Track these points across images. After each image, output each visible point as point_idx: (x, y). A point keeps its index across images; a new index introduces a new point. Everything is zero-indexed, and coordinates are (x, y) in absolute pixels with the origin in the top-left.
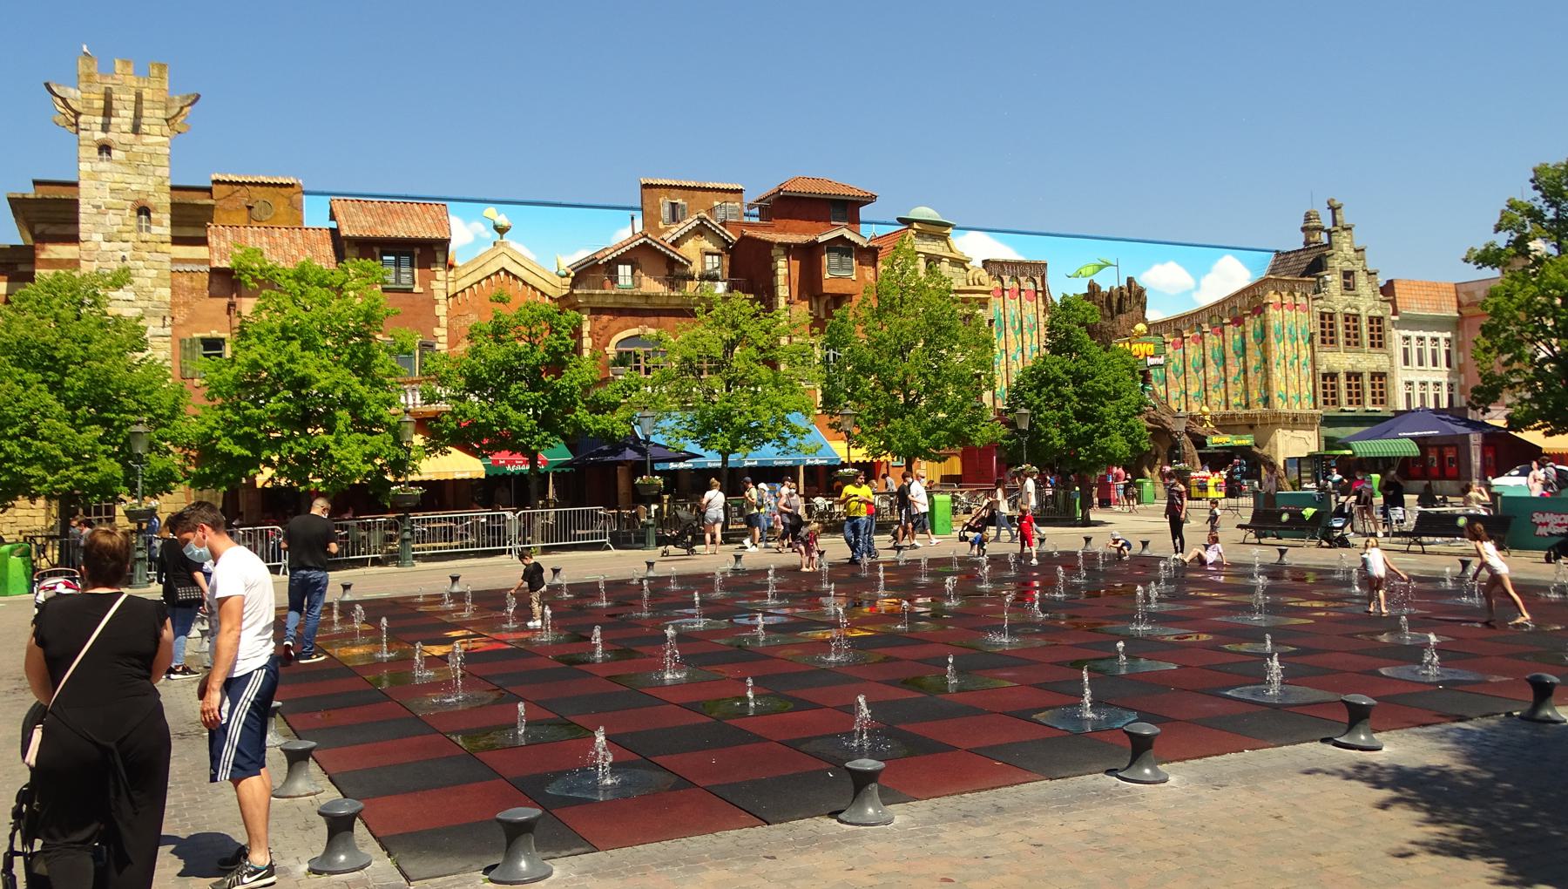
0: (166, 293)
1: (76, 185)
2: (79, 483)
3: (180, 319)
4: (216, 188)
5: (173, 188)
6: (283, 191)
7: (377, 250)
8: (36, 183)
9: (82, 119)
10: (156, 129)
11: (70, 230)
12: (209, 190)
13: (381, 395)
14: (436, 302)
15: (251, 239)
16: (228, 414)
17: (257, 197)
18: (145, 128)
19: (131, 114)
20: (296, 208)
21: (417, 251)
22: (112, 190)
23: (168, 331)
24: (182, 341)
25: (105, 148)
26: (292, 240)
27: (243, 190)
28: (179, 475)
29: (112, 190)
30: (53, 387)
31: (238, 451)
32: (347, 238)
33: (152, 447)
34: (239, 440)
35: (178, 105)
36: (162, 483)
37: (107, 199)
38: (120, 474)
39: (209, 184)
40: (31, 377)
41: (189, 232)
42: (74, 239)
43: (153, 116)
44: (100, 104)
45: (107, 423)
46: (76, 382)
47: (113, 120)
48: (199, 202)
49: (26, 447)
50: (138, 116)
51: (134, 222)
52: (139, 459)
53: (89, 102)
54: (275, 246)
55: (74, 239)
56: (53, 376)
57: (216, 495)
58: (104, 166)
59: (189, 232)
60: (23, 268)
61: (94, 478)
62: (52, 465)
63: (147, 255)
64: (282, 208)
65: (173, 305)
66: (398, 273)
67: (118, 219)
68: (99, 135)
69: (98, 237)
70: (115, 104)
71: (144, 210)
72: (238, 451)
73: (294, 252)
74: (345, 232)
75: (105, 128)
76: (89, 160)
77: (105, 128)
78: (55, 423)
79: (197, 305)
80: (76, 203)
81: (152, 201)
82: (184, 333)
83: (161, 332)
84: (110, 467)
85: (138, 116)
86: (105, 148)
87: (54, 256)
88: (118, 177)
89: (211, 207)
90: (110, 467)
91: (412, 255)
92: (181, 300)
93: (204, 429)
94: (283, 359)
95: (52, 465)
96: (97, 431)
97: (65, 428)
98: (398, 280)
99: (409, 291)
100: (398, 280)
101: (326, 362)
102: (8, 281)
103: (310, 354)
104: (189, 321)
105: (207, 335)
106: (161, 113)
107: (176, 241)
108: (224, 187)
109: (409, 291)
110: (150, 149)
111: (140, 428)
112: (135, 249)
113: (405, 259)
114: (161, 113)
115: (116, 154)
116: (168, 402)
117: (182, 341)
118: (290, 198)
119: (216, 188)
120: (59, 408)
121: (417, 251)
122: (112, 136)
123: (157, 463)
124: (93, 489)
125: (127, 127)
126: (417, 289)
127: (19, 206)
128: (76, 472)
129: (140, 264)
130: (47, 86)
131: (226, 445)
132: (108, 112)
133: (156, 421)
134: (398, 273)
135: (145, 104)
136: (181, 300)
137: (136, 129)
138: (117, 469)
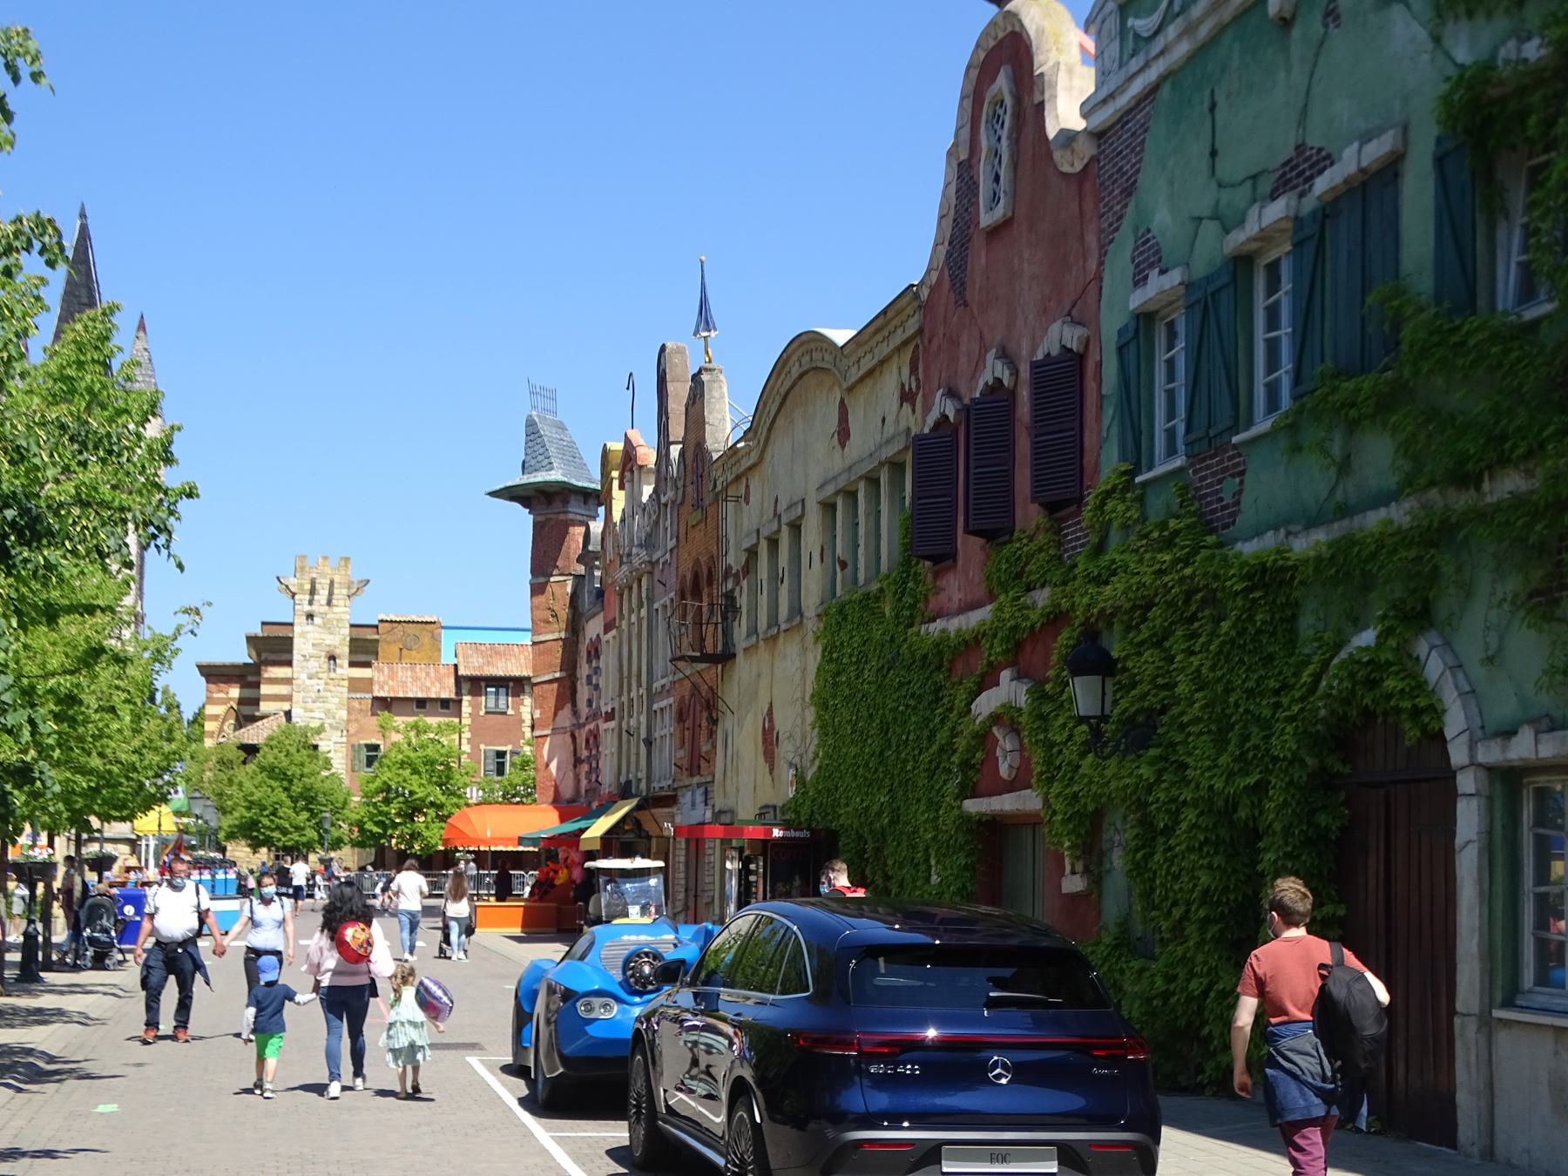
0: (343, 714)
1: (291, 624)
2: (297, 842)
3: (352, 731)
4: (381, 626)
5: (352, 626)
6: (428, 626)
7: (483, 684)
8: (264, 624)
9: (297, 597)
10: (342, 603)
11: (284, 657)
12: (376, 627)
13: (455, 800)
14: (523, 721)
15: (400, 674)
16: (371, 809)
17: (409, 631)
18: (334, 602)
19: (326, 592)
20: (436, 640)
21: (511, 684)
22: (314, 645)
23: (344, 739)
24: (353, 746)
25: (310, 616)
26: (428, 674)
27: (400, 627)
28: (346, 839)
29: (314, 645)
30: (286, 789)
31: (376, 829)
32: (463, 676)
33: (333, 825)
34: (377, 824)
35: (356, 586)
36: (337, 844)
37: (311, 651)
38: (316, 838)
39: (376, 623)
40: (275, 784)
41: (362, 658)
42: (289, 663)
43: (340, 592)
44: (308, 587)
45: (311, 811)
46: (297, 788)
47: (316, 597)
48: (369, 637)
49: (272, 821)
50: (331, 594)
51: (325, 666)
52: (326, 831)
53: (301, 585)
54: (416, 679)
55: (289, 663)
56: (285, 784)
57: (371, 853)
58: (310, 628)
59: (362, 658)
60: (250, 679)
61: (304, 839)
62: (285, 832)
63: (332, 688)
64: (426, 639)
65: (349, 721)
66: (497, 700)
67: (316, 664)
68: (307, 608)
69: (304, 676)
70: (317, 586)
71: (332, 658)
72: (376, 829)
73: (428, 684)
74: (462, 672)
75: (311, 603)
76: (300, 624)
77: (311, 603)
78: (286, 811)
79: (363, 721)
80: (291, 639)
81: (337, 651)
82: (354, 741)
83: (340, 740)
84: (311, 834)
85: (331, 594)
86: (310, 616)
87: (273, 676)
88: (317, 636)
89: (377, 641)
90: (311, 834)
91: (507, 688)
92: (353, 717)
93: (358, 817)
94: (401, 779)
95: (285, 832)
96: (305, 815)
97: (291, 813)
98: (497, 706)
99: (505, 713)
100: (497, 706)
101: (424, 782)
102: (241, 687)
103: (416, 777)
104: (358, 732)
105: (368, 742)
106: (345, 591)
107: (352, 664)
108: (387, 625)
109: (505, 713)
110: (338, 616)
111: (328, 815)
112: (326, 684)
113: (502, 691)
114: (345, 591)
115: (317, 620)
116: (341, 799)
117: (353, 746)
118: (432, 632)
119: (381, 626)
120: (288, 802)
121: (511, 684)
122: (315, 608)
123: (335, 833)
124: (304, 845)
125: (324, 602)
126: (510, 712)
127: (252, 640)
128: (295, 836)
129: (329, 694)
130: (278, 578)
131: (369, 826)
132: (313, 592)
133: (335, 812)
134: (497, 700)
135: (336, 585)
136: (353, 717)
137: (329, 603)
138: (315, 835)
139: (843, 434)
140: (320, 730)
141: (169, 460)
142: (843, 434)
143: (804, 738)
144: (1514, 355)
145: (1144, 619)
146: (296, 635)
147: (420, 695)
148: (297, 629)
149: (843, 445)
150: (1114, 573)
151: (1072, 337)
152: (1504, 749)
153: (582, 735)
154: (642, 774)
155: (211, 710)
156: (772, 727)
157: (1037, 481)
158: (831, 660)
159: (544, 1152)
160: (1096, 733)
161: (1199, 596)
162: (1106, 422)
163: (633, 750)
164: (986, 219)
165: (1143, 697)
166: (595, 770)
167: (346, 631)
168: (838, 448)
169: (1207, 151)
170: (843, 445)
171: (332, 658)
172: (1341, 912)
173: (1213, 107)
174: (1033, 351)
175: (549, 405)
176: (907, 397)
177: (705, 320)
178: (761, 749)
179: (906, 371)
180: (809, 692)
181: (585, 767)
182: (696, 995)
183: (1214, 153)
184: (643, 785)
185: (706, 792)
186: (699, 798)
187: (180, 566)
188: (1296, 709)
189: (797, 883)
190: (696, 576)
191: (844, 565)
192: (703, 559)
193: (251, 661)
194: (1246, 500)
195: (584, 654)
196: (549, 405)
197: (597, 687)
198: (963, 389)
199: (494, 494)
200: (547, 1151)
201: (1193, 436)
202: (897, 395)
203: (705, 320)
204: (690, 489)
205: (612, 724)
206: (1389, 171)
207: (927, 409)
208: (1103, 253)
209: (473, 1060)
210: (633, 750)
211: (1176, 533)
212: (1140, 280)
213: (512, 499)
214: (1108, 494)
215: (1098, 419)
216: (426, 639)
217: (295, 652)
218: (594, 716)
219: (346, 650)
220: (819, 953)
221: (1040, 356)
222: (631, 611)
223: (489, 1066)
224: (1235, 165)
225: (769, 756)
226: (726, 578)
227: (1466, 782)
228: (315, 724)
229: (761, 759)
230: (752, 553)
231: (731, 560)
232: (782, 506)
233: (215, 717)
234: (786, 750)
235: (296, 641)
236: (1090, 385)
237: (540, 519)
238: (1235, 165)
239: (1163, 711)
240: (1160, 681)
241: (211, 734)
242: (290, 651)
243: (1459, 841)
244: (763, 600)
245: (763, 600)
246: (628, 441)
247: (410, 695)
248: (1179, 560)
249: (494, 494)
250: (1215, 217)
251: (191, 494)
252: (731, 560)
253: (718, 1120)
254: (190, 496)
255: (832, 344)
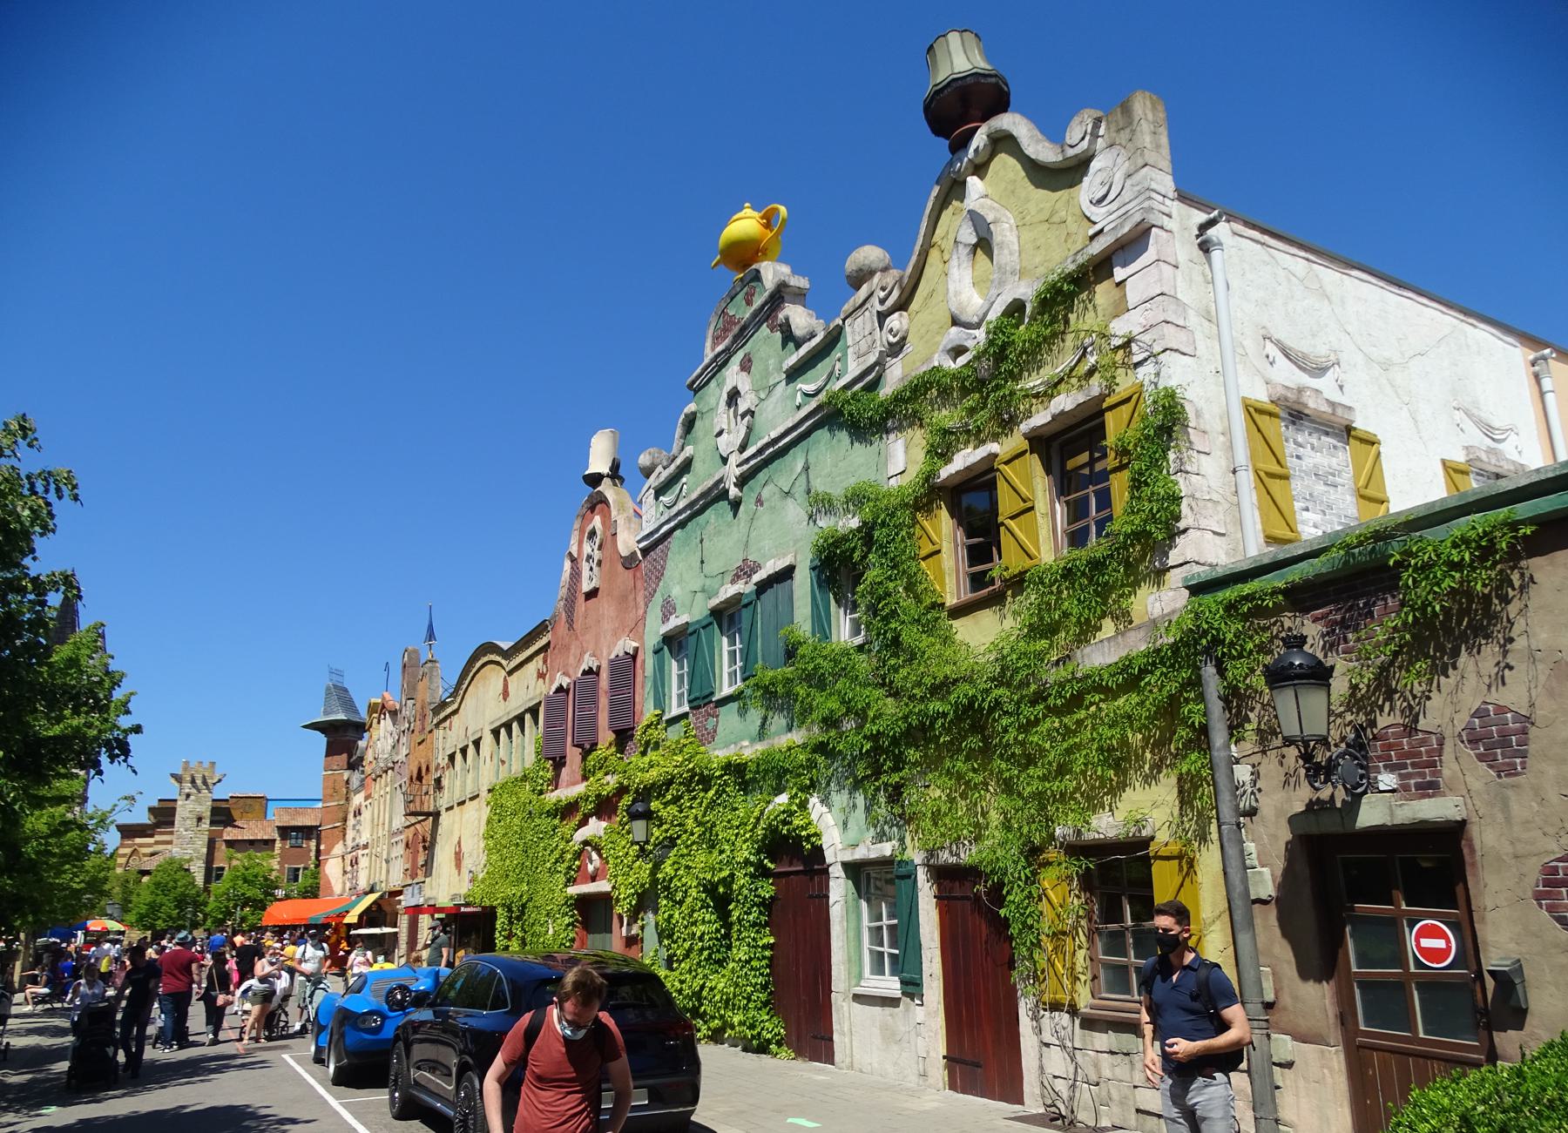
1: (176, 800)
8: (160, 800)
11: (170, 819)
64: (257, 807)
71: (200, 819)
127: (151, 810)
139: (506, 694)
140: (190, 860)
141: (128, 712)
142: (506, 694)
143: (478, 856)
144: (1500, 636)
145: (667, 790)
146: (178, 807)
147: (251, 838)
148: (179, 803)
149: (505, 699)
150: (652, 767)
151: (630, 645)
152: (852, 854)
153: (348, 858)
154: (383, 877)
155: (122, 851)
156: (460, 851)
157: (612, 719)
158: (495, 814)
159: (336, 1113)
160: (642, 849)
161: (697, 778)
162: (647, 690)
163: (378, 866)
164: (586, 587)
165: (667, 831)
166: (355, 877)
167: (210, 803)
168: (502, 701)
169: (699, 560)
170: (505, 699)
171: (200, 819)
172: (772, 941)
173: (701, 541)
174: (609, 654)
175: (340, 679)
176: (541, 675)
177: (431, 635)
178: (453, 863)
179: (541, 663)
180: (482, 832)
181: (349, 876)
182: (435, 1012)
183: (702, 562)
184: (383, 885)
185: (420, 888)
186: (416, 891)
187: (134, 772)
188: (748, 836)
189: (473, 937)
190: (420, 770)
191: (503, 762)
192: (423, 761)
193: (149, 822)
194: (720, 729)
195: (352, 814)
196: (340, 679)
197: (358, 831)
198: (571, 672)
199: (305, 727)
200: (337, 1113)
201: (692, 697)
202: (535, 675)
203: (431, 635)
204: (418, 723)
205: (366, 851)
206: (787, 574)
207: (552, 682)
208: (647, 606)
209: (286, 1057)
210: (378, 866)
211: (685, 746)
212: (665, 619)
213: (315, 729)
214: (648, 726)
215: (643, 687)
216: (257, 807)
217: (177, 816)
218: (357, 847)
219: (209, 813)
220: (511, 982)
221: (612, 656)
222: (381, 788)
223: (298, 1060)
224: (713, 567)
225: (458, 865)
226: (436, 770)
227: (836, 871)
228: (187, 857)
229: (454, 867)
230: (452, 757)
231: (440, 760)
232: (469, 732)
233: (123, 855)
234: (467, 863)
235: (178, 809)
236: (639, 671)
237: (331, 739)
238: (713, 567)
239: (679, 837)
240: (675, 822)
241: (120, 865)
242: (174, 815)
243: (831, 901)
244: (458, 783)
245: (458, 783)
246: (384, 698)
247: (246, 838)
248: (686, 760)
249: (305, 727)
250: (703, 591)
251: (137, 729)
252: (440, 760)
253: (450, 1088)
254: (137, 732)
255: (502, 649)
